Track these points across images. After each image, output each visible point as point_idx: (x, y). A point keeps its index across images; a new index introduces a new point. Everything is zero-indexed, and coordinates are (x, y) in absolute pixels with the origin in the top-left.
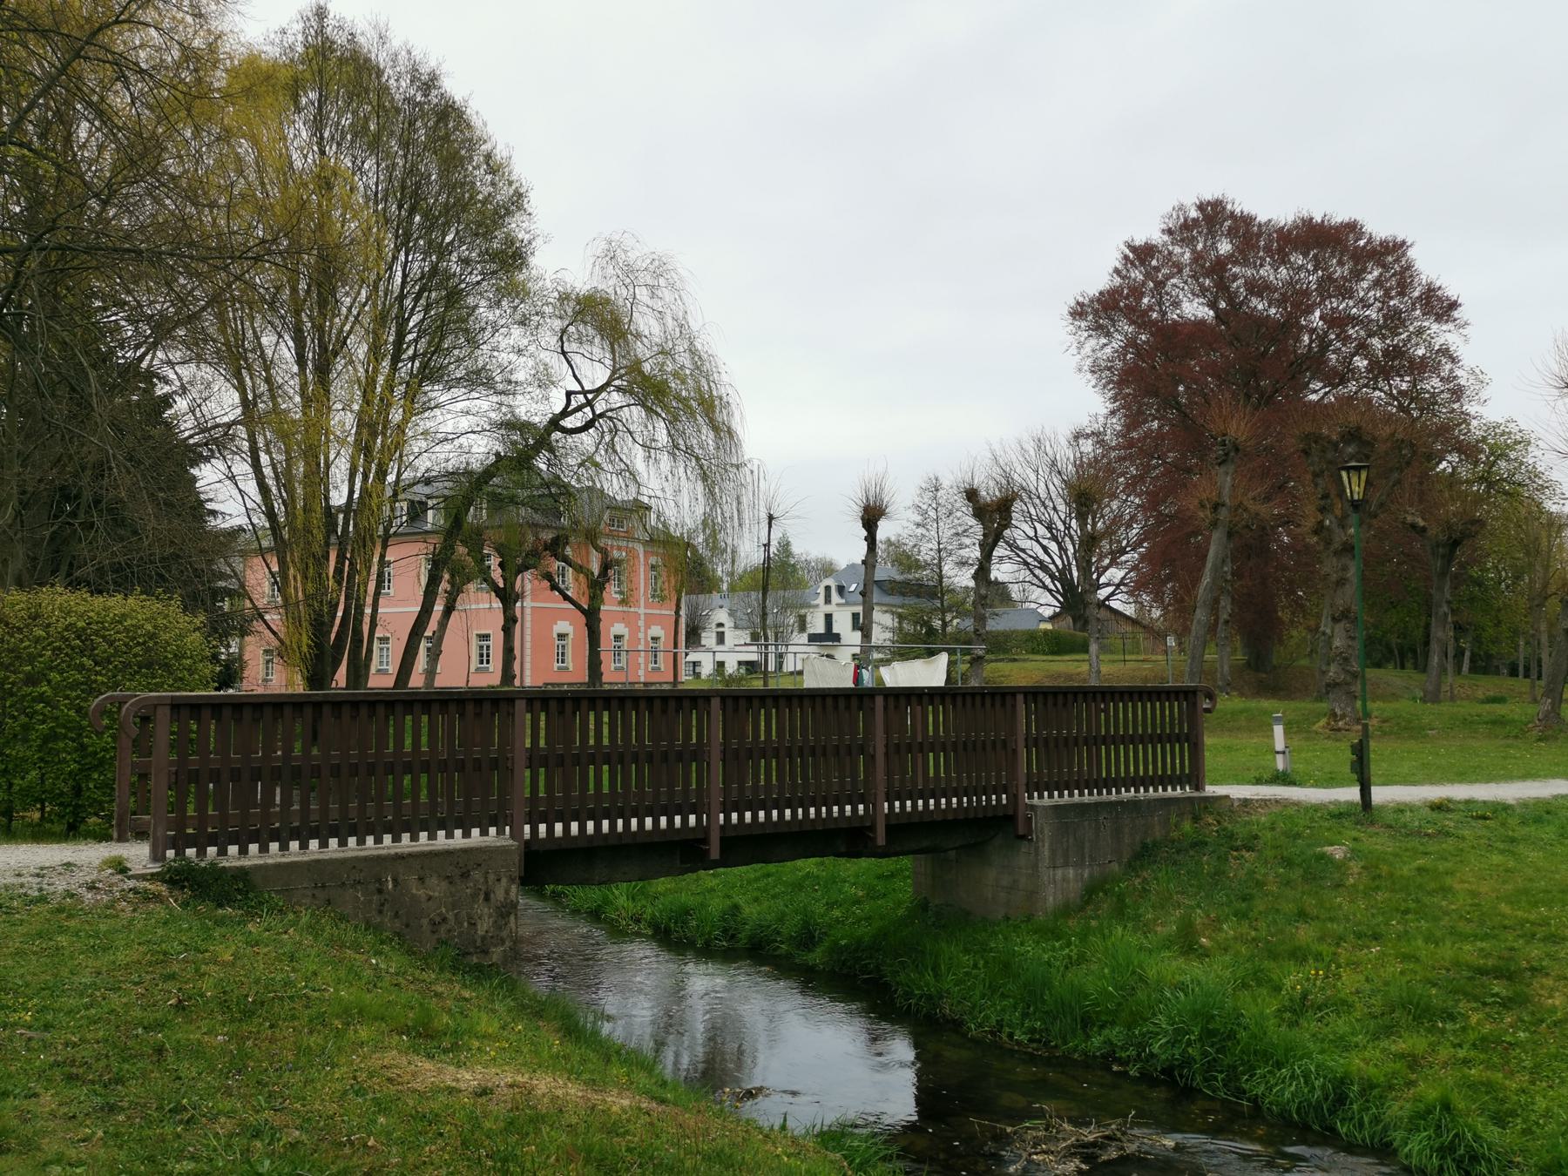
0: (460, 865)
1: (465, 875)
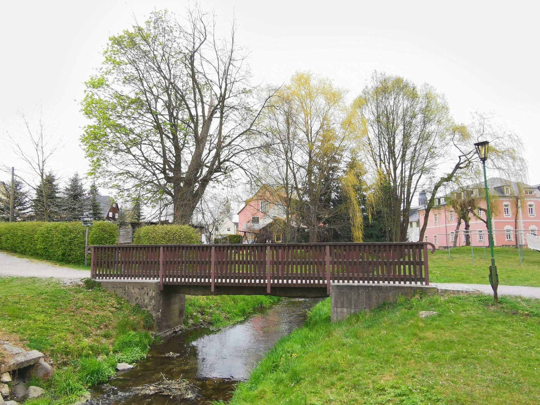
0: (142, 286)
1: (143, 288)
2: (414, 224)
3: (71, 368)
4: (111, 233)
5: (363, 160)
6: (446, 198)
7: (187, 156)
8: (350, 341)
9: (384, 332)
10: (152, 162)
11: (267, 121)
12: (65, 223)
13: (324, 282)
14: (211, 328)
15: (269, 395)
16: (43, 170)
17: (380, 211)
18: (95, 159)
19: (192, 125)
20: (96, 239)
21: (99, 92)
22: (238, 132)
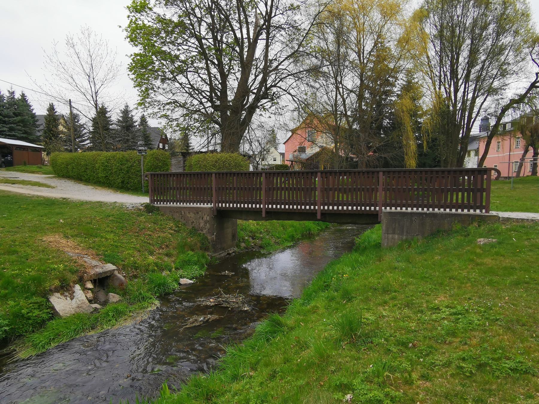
0: (197, 211)
1: (198, 213)
2: (472, 153)
3: (140, 280)
4: (164, 161)
5: (420, 82)
6: (513, 123)
7: (233, 83)
8: (402, 265)
9: (437, 258)
10: (197, 90)
11: (315, 41)
12: (121, 152)
13: (375, 209)
14: (262, 252)
15: (322, 310)
16: (96, 101)
17: (436, 139)
18: (143, 89)
19: (237, 49)
20: (151, 167)
21: (142, 17)
22: (284, 55)
